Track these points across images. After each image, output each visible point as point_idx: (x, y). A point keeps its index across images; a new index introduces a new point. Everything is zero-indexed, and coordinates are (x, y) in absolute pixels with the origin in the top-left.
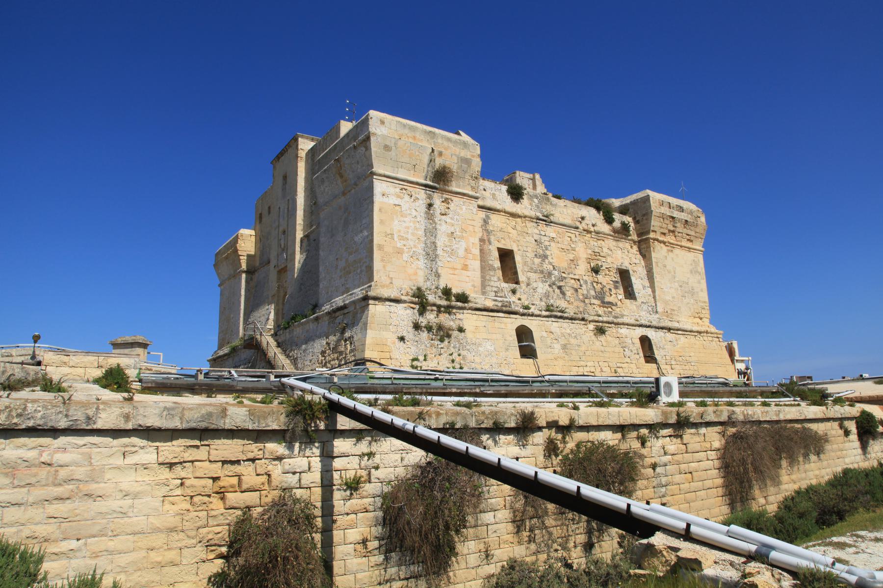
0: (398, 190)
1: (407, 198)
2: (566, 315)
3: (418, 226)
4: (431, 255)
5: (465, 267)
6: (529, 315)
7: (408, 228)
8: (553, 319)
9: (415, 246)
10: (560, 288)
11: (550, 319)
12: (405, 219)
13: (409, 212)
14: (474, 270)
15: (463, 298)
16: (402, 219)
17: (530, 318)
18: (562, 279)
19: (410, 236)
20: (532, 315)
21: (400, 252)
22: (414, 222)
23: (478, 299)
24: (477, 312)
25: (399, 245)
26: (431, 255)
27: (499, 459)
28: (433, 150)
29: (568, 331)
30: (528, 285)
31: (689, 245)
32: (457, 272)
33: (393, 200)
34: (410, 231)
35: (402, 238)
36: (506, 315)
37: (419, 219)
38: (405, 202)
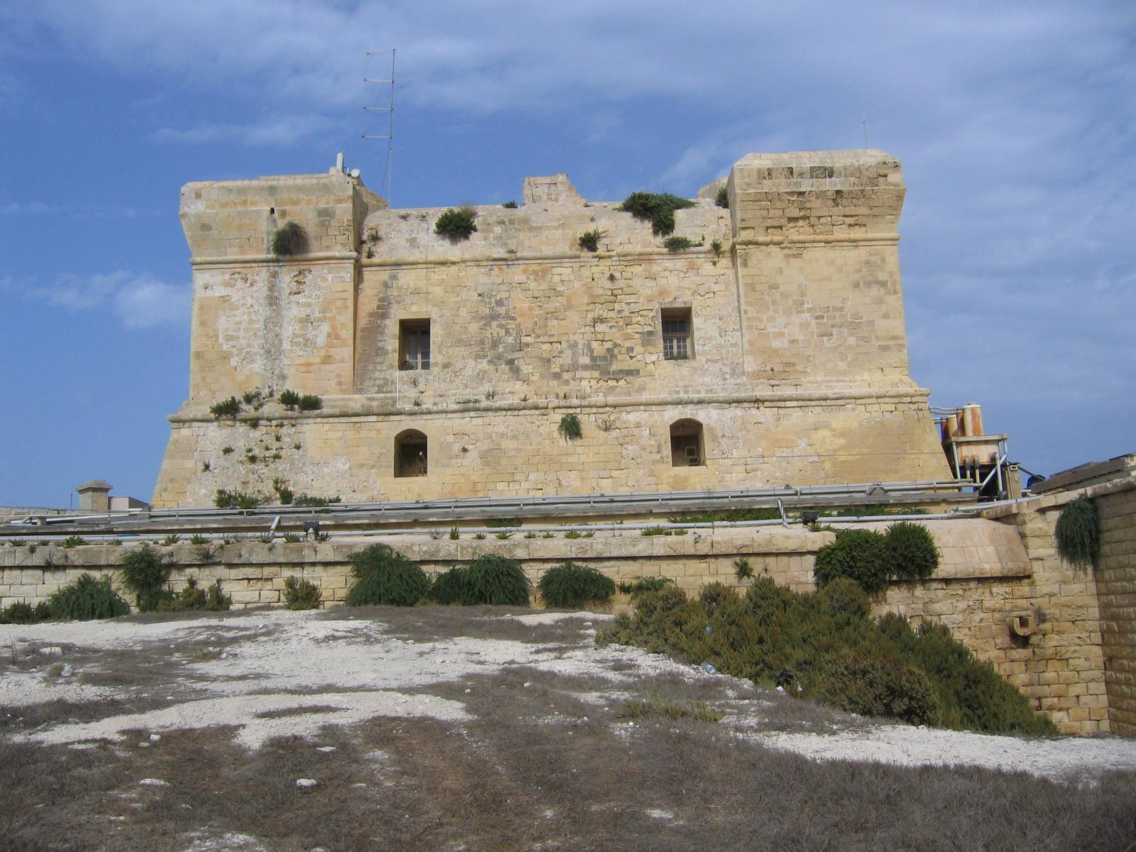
0: (227, 277)
1: (240, 284)
2: (191, 536)
3: (254, 317)
4: (272, 352)
5: (327, 360)
6: (422, 413)
7: (239, 323)
8: (472, 414)
9: (249, 345)
10: (511, 362)
11: (466, 414)
12: (237, 313)
13: (241, 302)
14: (342, 361)
15: (311, 404)
16: (232, 313)
17: (425, 417)
18: (521, 347)
19: (241, 334)
20: (429, 413)
21: (226, 357)
22: (249, 314)
23: (332, 397)
24: (331, 420)
25: (225, 348)
26: (272, 352)
27: (788, 264)
28: (272, 211)
29: (502, 429)
30: (446, 366)
31: (857, 233)
32: (312, 369)
33: (219, 291)
34: (243, 326)
35: (229, 338)
36: (381, 418)
37: (256, 308)
38: (236, 293)
